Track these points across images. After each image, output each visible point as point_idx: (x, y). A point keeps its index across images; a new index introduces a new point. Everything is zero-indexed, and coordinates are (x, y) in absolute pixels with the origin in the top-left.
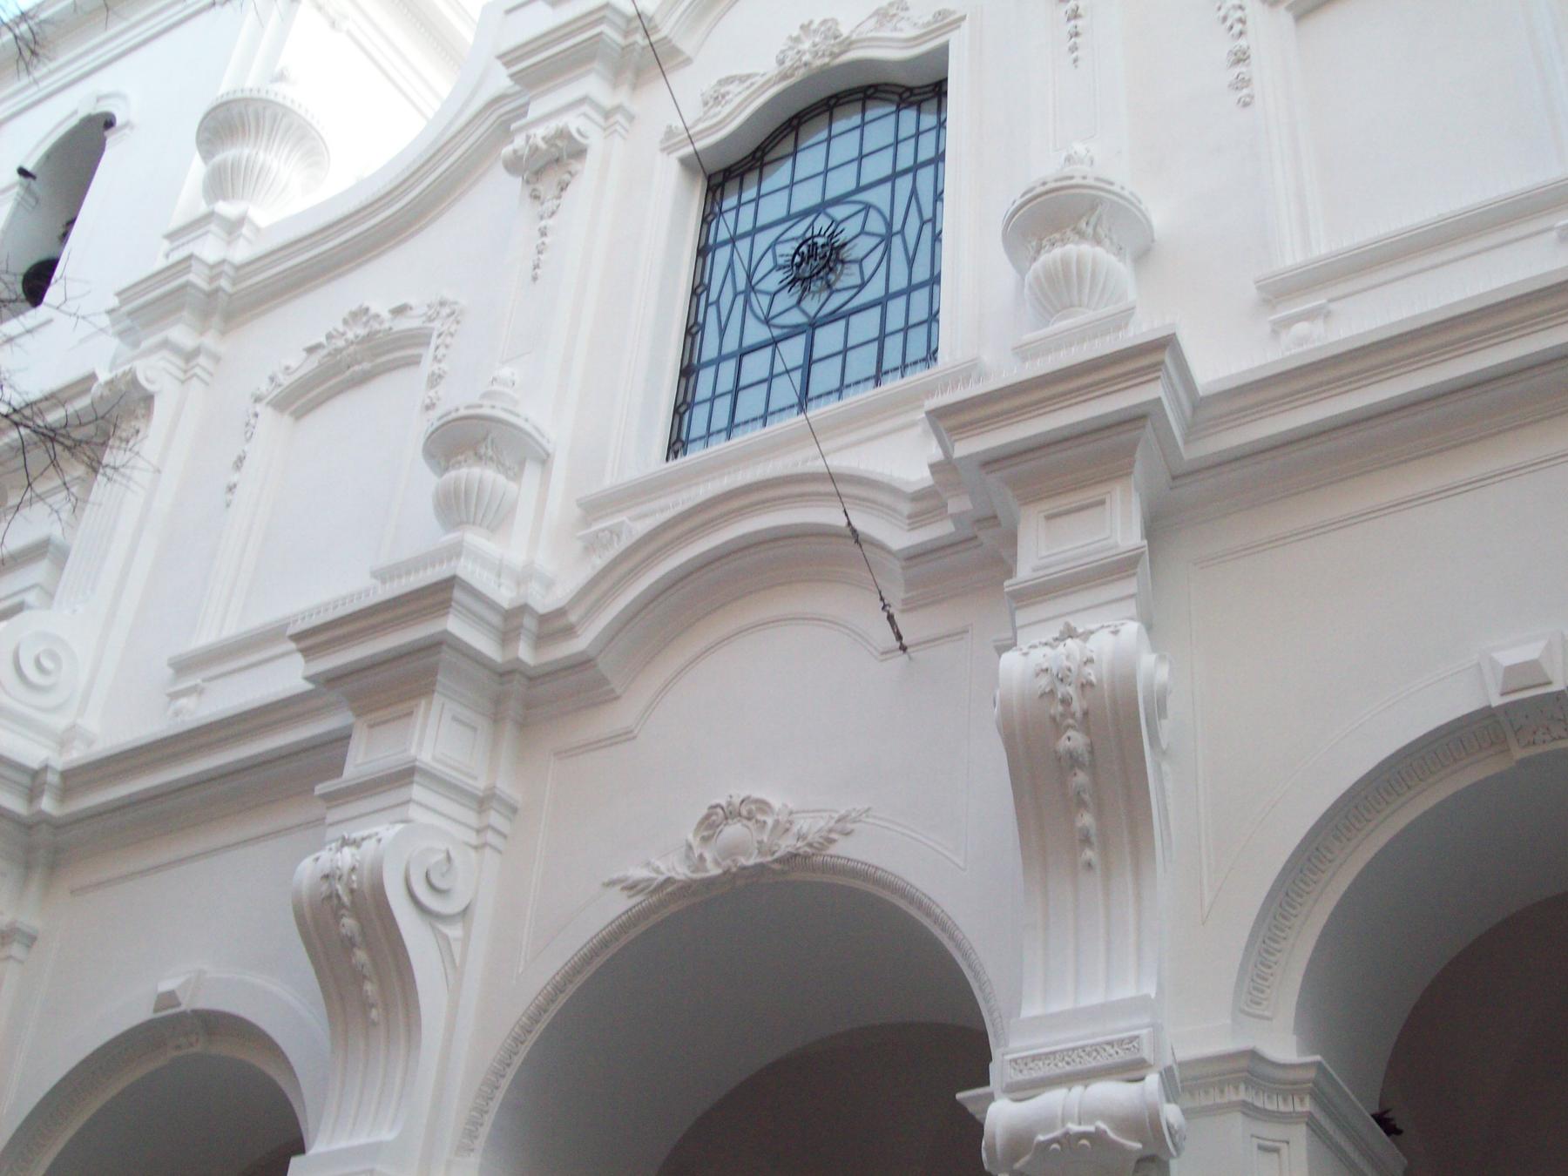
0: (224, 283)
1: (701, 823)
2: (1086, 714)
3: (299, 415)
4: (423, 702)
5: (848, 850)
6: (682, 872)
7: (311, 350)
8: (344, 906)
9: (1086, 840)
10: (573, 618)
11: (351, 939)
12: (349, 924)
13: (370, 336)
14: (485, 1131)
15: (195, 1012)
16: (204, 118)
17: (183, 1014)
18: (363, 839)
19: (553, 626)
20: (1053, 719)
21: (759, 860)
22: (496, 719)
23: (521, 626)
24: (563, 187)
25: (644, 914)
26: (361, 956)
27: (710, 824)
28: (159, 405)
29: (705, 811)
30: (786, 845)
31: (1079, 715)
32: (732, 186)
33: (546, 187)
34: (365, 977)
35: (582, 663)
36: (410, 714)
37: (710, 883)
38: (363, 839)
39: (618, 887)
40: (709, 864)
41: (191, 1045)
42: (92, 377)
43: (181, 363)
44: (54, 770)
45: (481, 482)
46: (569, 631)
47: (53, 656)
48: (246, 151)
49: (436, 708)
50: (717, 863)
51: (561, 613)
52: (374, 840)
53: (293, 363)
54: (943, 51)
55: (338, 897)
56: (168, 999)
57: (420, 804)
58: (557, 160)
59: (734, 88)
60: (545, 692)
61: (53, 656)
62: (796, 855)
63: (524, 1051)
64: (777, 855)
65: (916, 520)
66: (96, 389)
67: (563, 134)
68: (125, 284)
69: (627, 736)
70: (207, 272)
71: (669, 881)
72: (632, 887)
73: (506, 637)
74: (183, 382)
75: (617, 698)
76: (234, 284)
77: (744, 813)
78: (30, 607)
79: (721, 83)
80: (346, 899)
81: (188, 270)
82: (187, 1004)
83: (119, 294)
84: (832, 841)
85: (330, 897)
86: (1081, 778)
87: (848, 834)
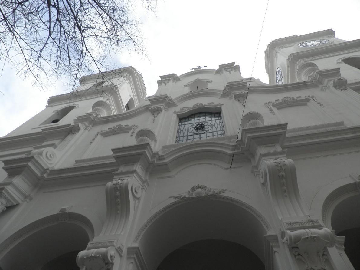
0: (45, 175)
1: (191, 189)
2: (285, 170)
3: (105, 137)
4: (136, 163)
5: (226, 194)
6: (187, 196)
7: (109, 129)
8: (118, 190)
9: (285, 192)
10: (165, 157)
11: (117, 196)
12: (118, 193)
13: (120, 128)
14: (140, 239)
15: (69, 213)
16: (95, 103)
17: (67, 212)
18: (124, 179)
19: (161, 158)
20: (278, 170)
21: (205, 195)
22: (146, 171)
23: (156, 156)
24: (158, 114)
25: (173, 204)
26: (119, 200)
27: (193, 189)
28: (80, 131)
29: (192, 187)
30: (210, 193)
31: (284, 169)
32: (184, 120)
33: (156, 114)
34: (118, 204)
35: (166, 164)
36: (133, 165)
37: (193, 198)
38: (124, 179)
39: (173, 198)
40: (194, 195)
41: (65, 220)
42: (70, 125)
43: (85, 127)
44: (49, 170)
45: (147, 139)
46: (164, 159)
47: (53, 155)
48: (101, 108)
49: (138, 166)
50: (195, 195)
51: (163, 156)
52: (126, 180)
53: (106, 130)
54: (128, 183)
55: (117, 188)
56: (65, 209)
57: (134, 177)
58: (158, 111)
59: (185, 109)
60: (157, 168)
61: (53, 155)
62: (213, 195)
63: (150, 224)
64: (208, 195)
65: (232, 150)
66: (70, 126)
67: (160, 108)
68: (78, 116)
69: (173, 176)
70: (93, 117)
71: (185, 197)
72: (176, 198)
73: (152, 158)
74: (85, 130)
75: (171, 171)
76: (97, 120)
77: (201, 187)
78: (105, 82)
79: (183, 108)
80: (119, 188)
81: (91, 116)
82: (68, 211)
83: (77, 117)
84: (220, 193)
85: (115, 188)
86: (284, 180)
87: (224, 192)
